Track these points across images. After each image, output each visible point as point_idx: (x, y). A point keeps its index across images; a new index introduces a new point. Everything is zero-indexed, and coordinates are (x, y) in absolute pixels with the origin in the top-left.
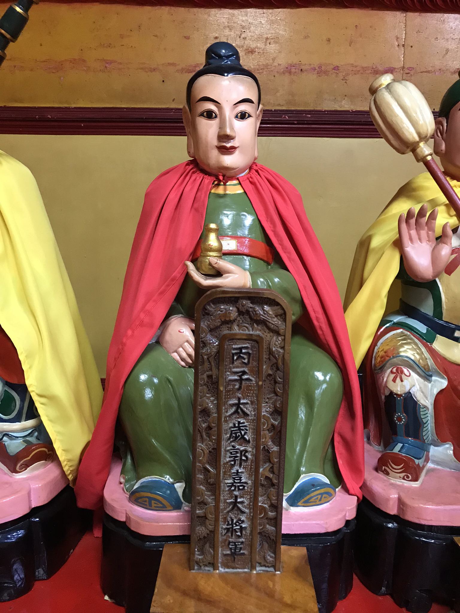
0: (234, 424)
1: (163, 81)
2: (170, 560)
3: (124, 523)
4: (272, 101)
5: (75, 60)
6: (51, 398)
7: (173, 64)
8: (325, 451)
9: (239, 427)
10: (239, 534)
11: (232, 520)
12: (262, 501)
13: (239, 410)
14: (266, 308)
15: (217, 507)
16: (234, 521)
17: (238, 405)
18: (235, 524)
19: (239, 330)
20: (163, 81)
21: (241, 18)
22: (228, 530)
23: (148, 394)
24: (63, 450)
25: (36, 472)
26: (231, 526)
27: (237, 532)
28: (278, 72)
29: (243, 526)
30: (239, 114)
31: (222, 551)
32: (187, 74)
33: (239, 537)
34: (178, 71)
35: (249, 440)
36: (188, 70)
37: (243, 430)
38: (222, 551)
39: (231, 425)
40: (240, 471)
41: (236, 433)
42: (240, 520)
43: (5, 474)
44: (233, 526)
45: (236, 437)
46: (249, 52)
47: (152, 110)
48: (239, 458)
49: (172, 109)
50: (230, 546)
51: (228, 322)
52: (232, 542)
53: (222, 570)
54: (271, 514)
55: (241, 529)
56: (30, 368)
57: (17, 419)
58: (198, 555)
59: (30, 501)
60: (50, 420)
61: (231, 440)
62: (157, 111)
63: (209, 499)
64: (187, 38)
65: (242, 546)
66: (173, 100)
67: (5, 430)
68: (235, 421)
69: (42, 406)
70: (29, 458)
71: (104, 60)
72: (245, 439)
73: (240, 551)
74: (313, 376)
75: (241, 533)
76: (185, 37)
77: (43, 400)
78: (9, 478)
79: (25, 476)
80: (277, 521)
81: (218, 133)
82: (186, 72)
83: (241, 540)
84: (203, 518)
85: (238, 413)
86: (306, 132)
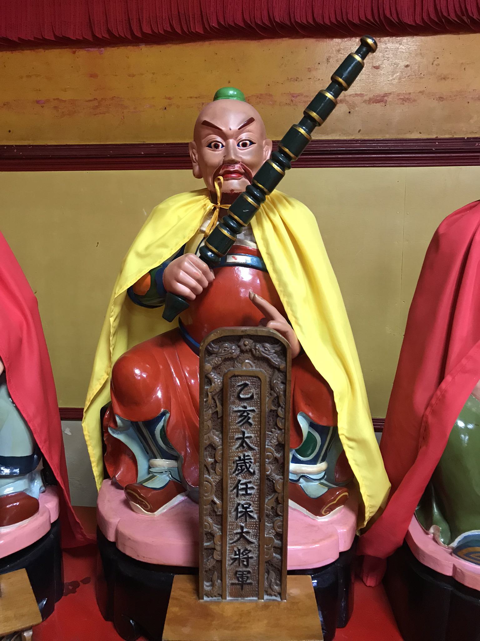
0: (240, 457)
1: (350, 112)
2: (180, 586)
3: (114, 544)
4: (464, 129)
5: (261, 95)
6: (361, 443)
7: (361, 95)
9: (244, 460)
10: (245, 563)
11: (239, 550)
12: (269, 534)
13: (244, 445)
14: (267, 345)
16: (242, 551)
17: (243, 439)
18: (242, 553)
19: (256, 367)
20: (350, 112)
21: (383, 46)
22: (235, 559)
24: (368, 496)
25: (335, 516)
26: (238, 557)
27: (244, 561)
28: (472, 98)
30: (241, 143)
31: (229, 580)
32: (375, 104)
33: (247, 566)
34: (365, 101)
35: (254, 472)
36: (376, 100)
37: (248, 463)
38: (229, 580)
39: (237, 459)
41: (241, 466)
42: (247, 550)
43: (305, 516)
45: (242, 470)
46: (441, 79)
47: (341, 142)
48: (242, 466)
49: (30, 146)
50: (238, 576)
52: (240, 572)
54: (277, 542)
55: (248, 559)
56: (341, 410)
57: (314, 462)
58: (207, 586)
59: (50, 521)
60: (357, 465)
61: (237, 472)
62: (345, 142)
63: (216, 529)
64: (377, 68)
65: (249, 575)
66: (359, 131)
67: (304, 471)
69: (350, 450)
70: (335, 502)
71: (291, 94)
72: (250, 472)
73: (247, 580)
75: (248, 562)
76: (374, 67)
77: (352, 444)
78: (313, 521)
79: (326, 520)
80: (282, 550)
82: (373, 102)
83: (248, 569)
86: (317, 163)
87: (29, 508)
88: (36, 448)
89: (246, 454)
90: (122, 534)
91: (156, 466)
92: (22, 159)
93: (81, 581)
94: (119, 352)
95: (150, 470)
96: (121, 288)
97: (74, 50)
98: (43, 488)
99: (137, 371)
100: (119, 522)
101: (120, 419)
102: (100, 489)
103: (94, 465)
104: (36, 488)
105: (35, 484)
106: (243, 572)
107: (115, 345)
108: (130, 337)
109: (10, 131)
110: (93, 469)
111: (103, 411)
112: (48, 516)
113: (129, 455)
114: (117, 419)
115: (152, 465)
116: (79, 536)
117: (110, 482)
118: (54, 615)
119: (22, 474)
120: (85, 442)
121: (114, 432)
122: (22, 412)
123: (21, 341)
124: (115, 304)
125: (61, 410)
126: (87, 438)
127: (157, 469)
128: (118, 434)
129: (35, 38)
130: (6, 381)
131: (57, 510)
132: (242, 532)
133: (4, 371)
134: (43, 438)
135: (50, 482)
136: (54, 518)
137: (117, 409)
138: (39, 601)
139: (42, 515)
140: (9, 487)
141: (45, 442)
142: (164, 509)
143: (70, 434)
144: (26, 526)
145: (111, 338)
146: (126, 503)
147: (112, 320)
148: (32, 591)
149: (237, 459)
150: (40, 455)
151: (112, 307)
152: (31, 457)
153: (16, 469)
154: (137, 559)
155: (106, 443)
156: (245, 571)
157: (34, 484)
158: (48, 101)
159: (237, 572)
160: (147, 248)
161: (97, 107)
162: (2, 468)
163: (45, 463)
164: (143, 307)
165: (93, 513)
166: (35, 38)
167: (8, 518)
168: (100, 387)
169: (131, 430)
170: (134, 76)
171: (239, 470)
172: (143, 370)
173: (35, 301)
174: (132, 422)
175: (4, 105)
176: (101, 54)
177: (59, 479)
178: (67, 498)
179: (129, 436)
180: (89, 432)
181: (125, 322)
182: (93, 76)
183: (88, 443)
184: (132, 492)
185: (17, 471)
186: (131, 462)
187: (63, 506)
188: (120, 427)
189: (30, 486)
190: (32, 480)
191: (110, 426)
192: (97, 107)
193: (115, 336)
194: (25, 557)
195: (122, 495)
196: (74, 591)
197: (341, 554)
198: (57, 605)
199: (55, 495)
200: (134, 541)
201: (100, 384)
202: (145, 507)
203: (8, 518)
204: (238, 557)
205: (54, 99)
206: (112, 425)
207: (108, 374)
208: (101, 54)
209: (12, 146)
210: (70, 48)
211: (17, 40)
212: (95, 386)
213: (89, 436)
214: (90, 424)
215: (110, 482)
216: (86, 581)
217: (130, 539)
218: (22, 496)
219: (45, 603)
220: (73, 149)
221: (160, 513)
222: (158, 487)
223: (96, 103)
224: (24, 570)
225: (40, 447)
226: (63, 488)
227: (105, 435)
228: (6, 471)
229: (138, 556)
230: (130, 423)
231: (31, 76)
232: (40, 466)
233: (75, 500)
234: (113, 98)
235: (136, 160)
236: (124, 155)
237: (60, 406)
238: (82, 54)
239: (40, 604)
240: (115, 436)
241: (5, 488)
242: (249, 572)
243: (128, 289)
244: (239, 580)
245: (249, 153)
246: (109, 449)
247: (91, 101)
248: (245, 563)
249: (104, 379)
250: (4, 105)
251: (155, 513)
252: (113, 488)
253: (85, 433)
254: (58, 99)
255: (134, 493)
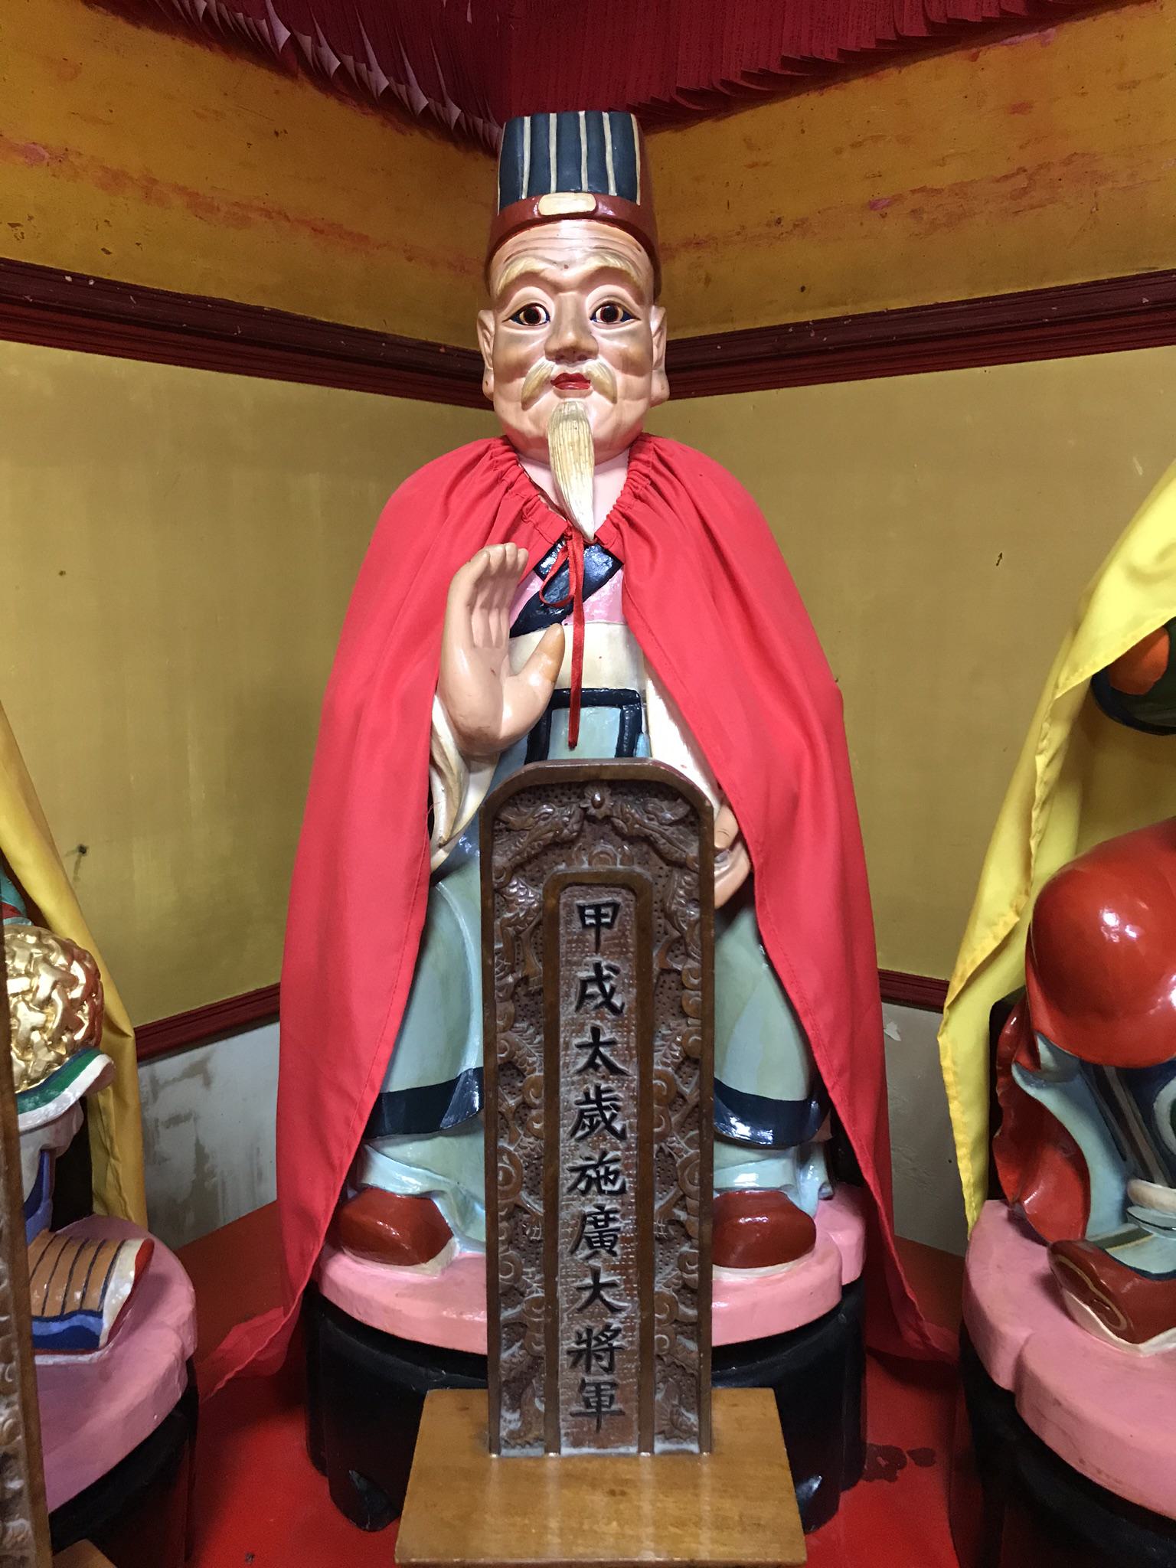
0: (587, 1094)
2: (444, 1419)
3: (1009, 1398)
8: (579, 880)
9: (599, 1100)
10: (605, 1363)
11: (589, 1331)
13: (598, 1061)
15: (551, 1299)
16: (595, 1332)
18: (597, 1339)
23: (1132, 933)
26: (584, 1346)
27: (599, 1358)
29: (615, 1344)
30: (598, 313)
37: (607, 1108)
38: (570, 1405)
40: (603, 1086)
41: (591, 1118)
42: (608, 1327)
44: (589, 1345)
45: (592, 1128)
49: (846, 318)
51: (561, 844)
53: (566, 1451)
61: (580, 1133)
68: (594, 1080)
72: (613, 1131)
74: (1100, 923)
80: (701, 1326)
81: (797, 1497)
83: (606, 1378)
84: (518, 1328)
85: (596, 1067)
87: (788, 1237)
88: (816, 1084)
89: (603, 1086)
90: (1036, 1382)
91: (1151, 1205)
92: (825, 352)
93: (910, 1453)
94: (1054, 856)
95: (1131, 1210)
96: (1075, 669)
97: (974, 50)
98: (828, 1190)
99: (1110, 919)
100: (1027, 1341)
101: (1050, 1048)
102: (977, 1223)
103: (962, 1152)
104: (810, 1186)
105: (809, 1176)
106: (598, 1385)
107: (1043, 833)
108: (1088, 814)
109: (803, 289)
110: (961, 1165)
111: (999, 1013)
112: (836, 1269)
113: (1065, 1151)
114: (1041, 1047)
115: (1137, 1198)
116: (911, 1336)
117: (1004, 1212)
118: (836, 1526)
119: (778, 1147)
120: (942, 1086)
121: (1028, 1083)
122: (787, 986)
123: (795, 802)
124: (1053, 717)
125: (886, 977)
126: (948, 1077)
127: (1153, 1213)
128: (1039, 1087)
129: (878, 41)
130: (754, 903)
131: (860, 1255)
132: (596, 1043)
133: (750, 876)
134: (836, 1062)
135: (844, 1177)
136: (851, 1273)
137: (1043, 1018)
138: (799, 1476)
139: (821, 1262)
140: (748, 1172)
141: (840, 1074)
142: (1169, 1340)
143: (896, 1037)
144: (780, 1280)
145: (1035, 814)
146: (1051, 1287)
147: (1041, 761)
148: (785, 1461)
149: (581, 1097)
150: (827, 1105)
151: (1046, 725)
152: (803, 1105)
153: (765, 1130)
154: (1079, 1470)
155: (1001, 1103)
156: (605, 1383)
157: (805, 1175)
158: (898, 199)
159: (584, 1384)
160: (1163, 555)
161: (1024, 191)
162: (733, 1120)
163: (837, 1126)
164: (1132, 730)
165: (949, 1269)
166: (878, 41)
167: (740, 1249)
168: (995, 944)
169: (1078, 1083)
170: (1134, 84)
171: (584, 1125)
172: (1129, 915)
173: (837, 700)
174: (1084, 1064)
175: (795, 226)
176: (1044, 44)
177: (869, 1177)
178: (884, 1219)
179: (1068, 1095)
180: (954, 1063)
181: (1079, 768)
182: (1020, 108)
183: (951, 1092)
184: (1072, 1266)
185: (768, 1135)
186: (1069, 1172)
187: (874, 1246)
188: (1047, 1071)
189: (795, 1178)
190: (802, 1161)
191: (1016, 1062)
192: (1024, 191)
193: (1047, 807)
194: (773, 1359)
195: (1040, 1260)
196: (889, 1474)
197: (846, 1290)
198: (845, 1498)
199: (855, 1214)
200: (1070, 1413)
201: (995, 937)
202: (1111, 1321)
203: (740, 1249)
204: (584, 1346)
205: (913, 192)
206: (1024, 1059)
207: (1018, 913)
208: (1044, 44)
209: (807, 323)
210: (963, 48)
211: (833, 57)
212: (981, 943)
213: (955, 1073)
214: (961, 1038)
215: (1004, 1212)
216: (924, 1458)
217: (1058, 1403)
218: (775, 1200)
219: (816, 1486)
220: (951, 312)
221: (1156, 1350)
222: (1155, 1270)
223: (1021, 181)
224: (770, 1392)
225: (828, 1084)
226: (879, 1202)
227: (1001, 1080)
228: (742, 1130)
229: (1081, 1461)
230: (1075, 1063)
231: (860, 144)
232: (824, 1134)
233: (908, 1223)
234: (1068, 161)
235: (1133, 320)
236: (1092, 311)
237: (880, 967)
238: (996, 56)
239: (804, 1488)
240: (1031, 1091)
241: (739, 1172)
242: (613, 1385)
243: (1095, 677)
244: (588, 1406)
245: (438, 1293)
246: (1010, 1122)
247: (1006, 177)
248: (605, 1363)
249: (1006, 923)
250: (795, 226)
251: (1141, 1346)
252: (1011, 1233)
253: (946, 1063)
254: (922, 190)
255: (1079, 1272)
